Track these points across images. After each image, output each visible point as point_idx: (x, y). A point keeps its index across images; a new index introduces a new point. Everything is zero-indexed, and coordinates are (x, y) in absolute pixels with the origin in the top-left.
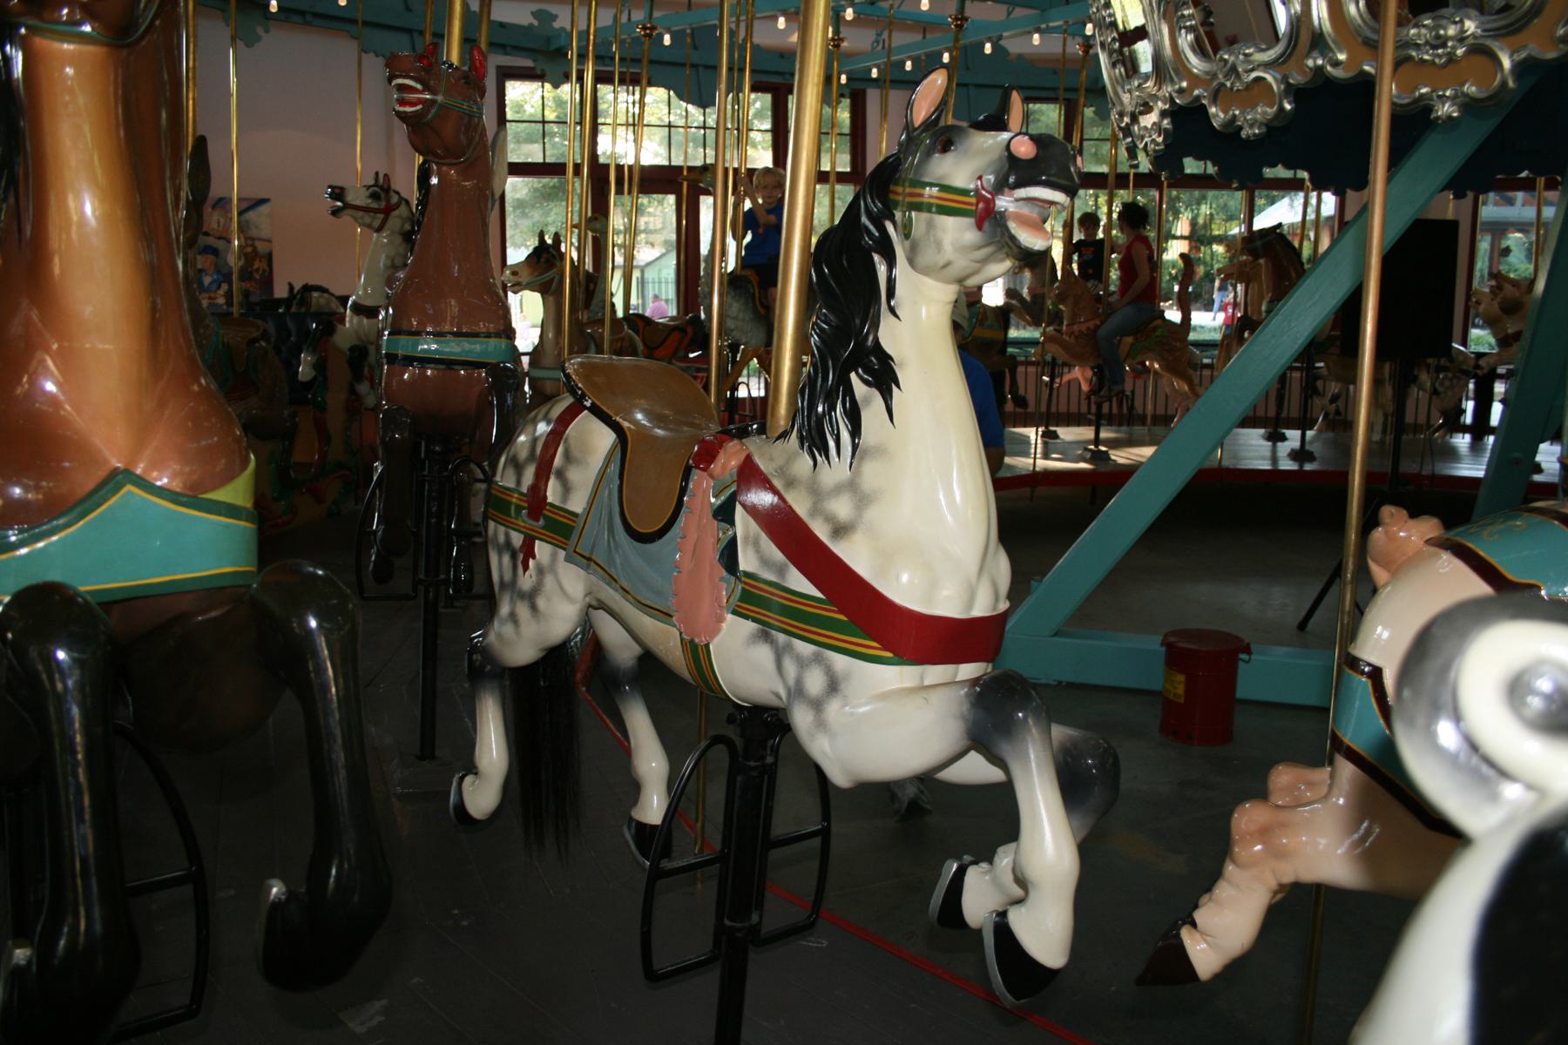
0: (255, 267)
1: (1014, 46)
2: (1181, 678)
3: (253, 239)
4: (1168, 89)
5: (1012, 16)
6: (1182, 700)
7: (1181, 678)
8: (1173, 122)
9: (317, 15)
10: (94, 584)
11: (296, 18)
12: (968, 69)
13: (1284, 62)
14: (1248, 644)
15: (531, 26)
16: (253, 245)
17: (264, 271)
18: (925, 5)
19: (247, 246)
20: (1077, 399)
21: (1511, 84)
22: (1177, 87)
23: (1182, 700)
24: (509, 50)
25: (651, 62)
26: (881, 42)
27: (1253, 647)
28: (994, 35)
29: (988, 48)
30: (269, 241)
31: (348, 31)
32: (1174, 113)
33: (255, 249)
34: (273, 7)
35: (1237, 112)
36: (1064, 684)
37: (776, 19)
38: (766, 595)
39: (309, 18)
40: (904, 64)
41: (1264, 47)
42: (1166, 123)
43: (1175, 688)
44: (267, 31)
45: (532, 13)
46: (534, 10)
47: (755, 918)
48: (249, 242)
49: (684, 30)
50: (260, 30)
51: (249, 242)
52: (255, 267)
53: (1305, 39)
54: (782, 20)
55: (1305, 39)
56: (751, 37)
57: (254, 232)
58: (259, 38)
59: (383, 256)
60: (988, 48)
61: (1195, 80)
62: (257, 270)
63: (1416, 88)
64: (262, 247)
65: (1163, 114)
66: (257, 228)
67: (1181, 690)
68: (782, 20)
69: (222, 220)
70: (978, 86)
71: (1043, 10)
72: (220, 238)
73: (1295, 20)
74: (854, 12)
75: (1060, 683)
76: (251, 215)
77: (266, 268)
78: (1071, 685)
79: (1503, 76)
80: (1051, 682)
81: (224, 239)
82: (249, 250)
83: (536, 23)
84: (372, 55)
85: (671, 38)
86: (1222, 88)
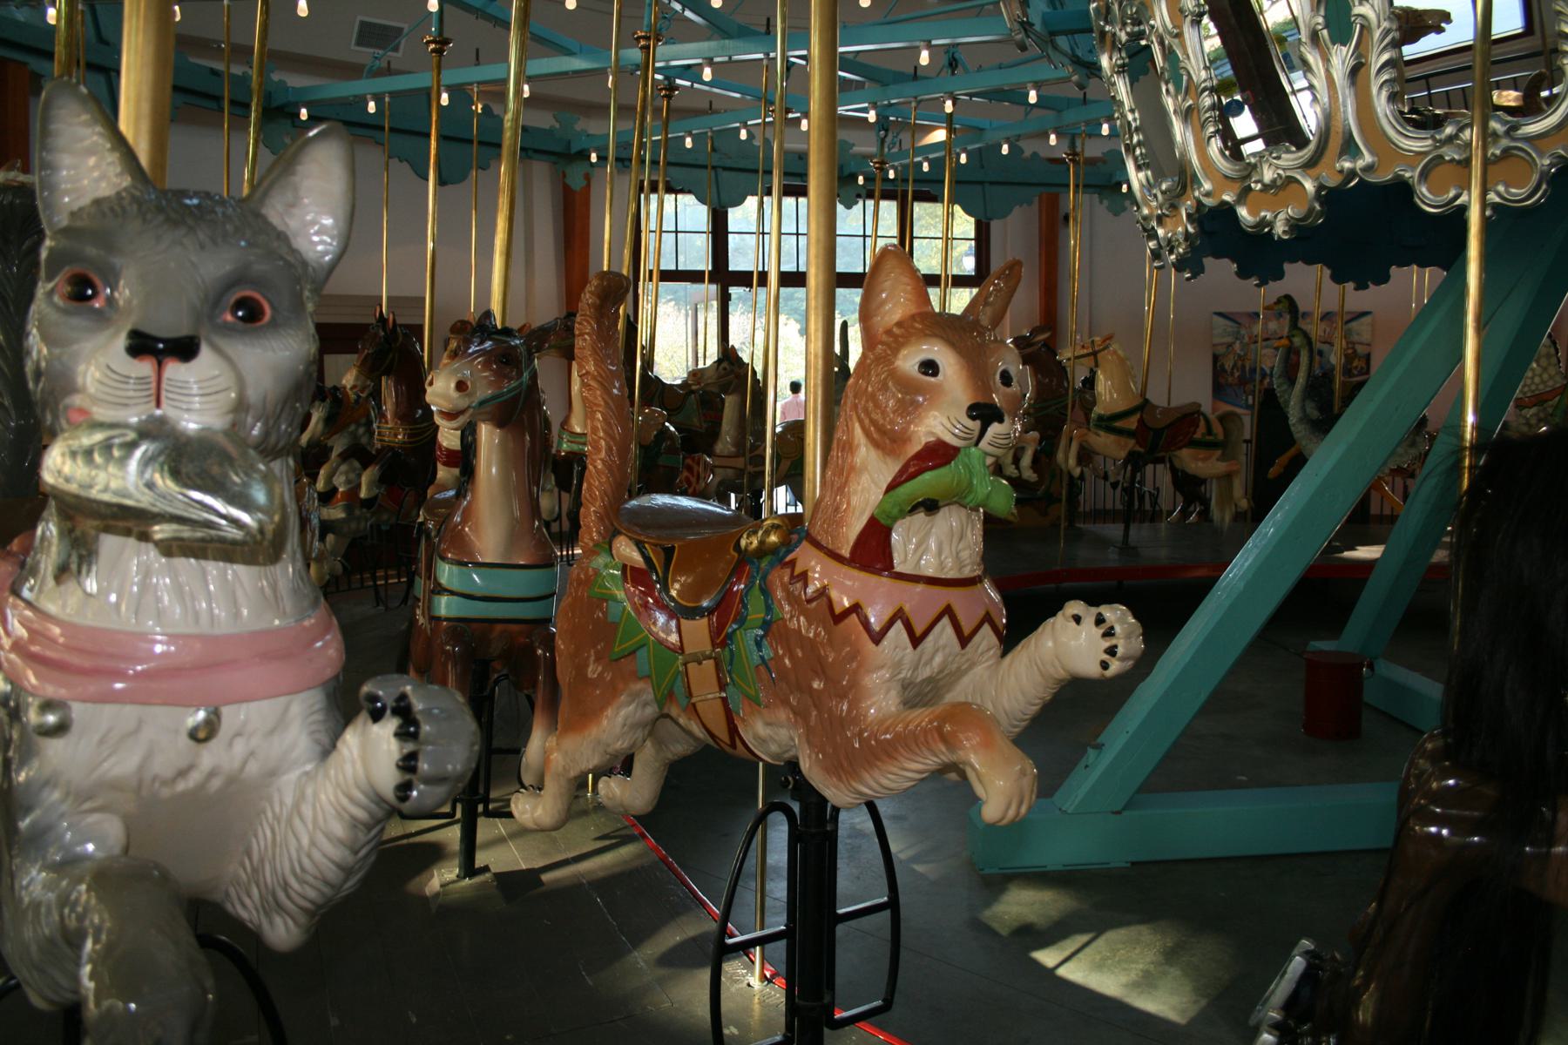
0: (1354, 364)
1: (1028, 148)
3: (1354, 343)
5: (1028, 117)
16: (1353, 348)
17: (1362, 368)
19: (1348, 348)
25: (705, 167)
26: (898, 144)
29: (1005, 149)
30: (1369, 345)
33: (1355, 351)
38: (388, 846)
40: (683, 139)
48: (1350, 346)
49: (706, 133)
51: (1350, 346)
52: (1354, 364)
53: (1335, 143)
54: (1053, 137)
55: (1335, 143)
57: (1355, 338)
60: (1005, 149)
62: (1356, 367)
64: (1360, 349)
66: (1358, 334)
68: (1053, 137)
69: (1328, 330)
70: (992, 183)
71: (1059, 111)
72: (1324, 343)
76: (1354, 324)
77: (1364, 365)
81: (1329, 343)
82: (1350, 351)
84: (396, 160)
85: (693, 141)
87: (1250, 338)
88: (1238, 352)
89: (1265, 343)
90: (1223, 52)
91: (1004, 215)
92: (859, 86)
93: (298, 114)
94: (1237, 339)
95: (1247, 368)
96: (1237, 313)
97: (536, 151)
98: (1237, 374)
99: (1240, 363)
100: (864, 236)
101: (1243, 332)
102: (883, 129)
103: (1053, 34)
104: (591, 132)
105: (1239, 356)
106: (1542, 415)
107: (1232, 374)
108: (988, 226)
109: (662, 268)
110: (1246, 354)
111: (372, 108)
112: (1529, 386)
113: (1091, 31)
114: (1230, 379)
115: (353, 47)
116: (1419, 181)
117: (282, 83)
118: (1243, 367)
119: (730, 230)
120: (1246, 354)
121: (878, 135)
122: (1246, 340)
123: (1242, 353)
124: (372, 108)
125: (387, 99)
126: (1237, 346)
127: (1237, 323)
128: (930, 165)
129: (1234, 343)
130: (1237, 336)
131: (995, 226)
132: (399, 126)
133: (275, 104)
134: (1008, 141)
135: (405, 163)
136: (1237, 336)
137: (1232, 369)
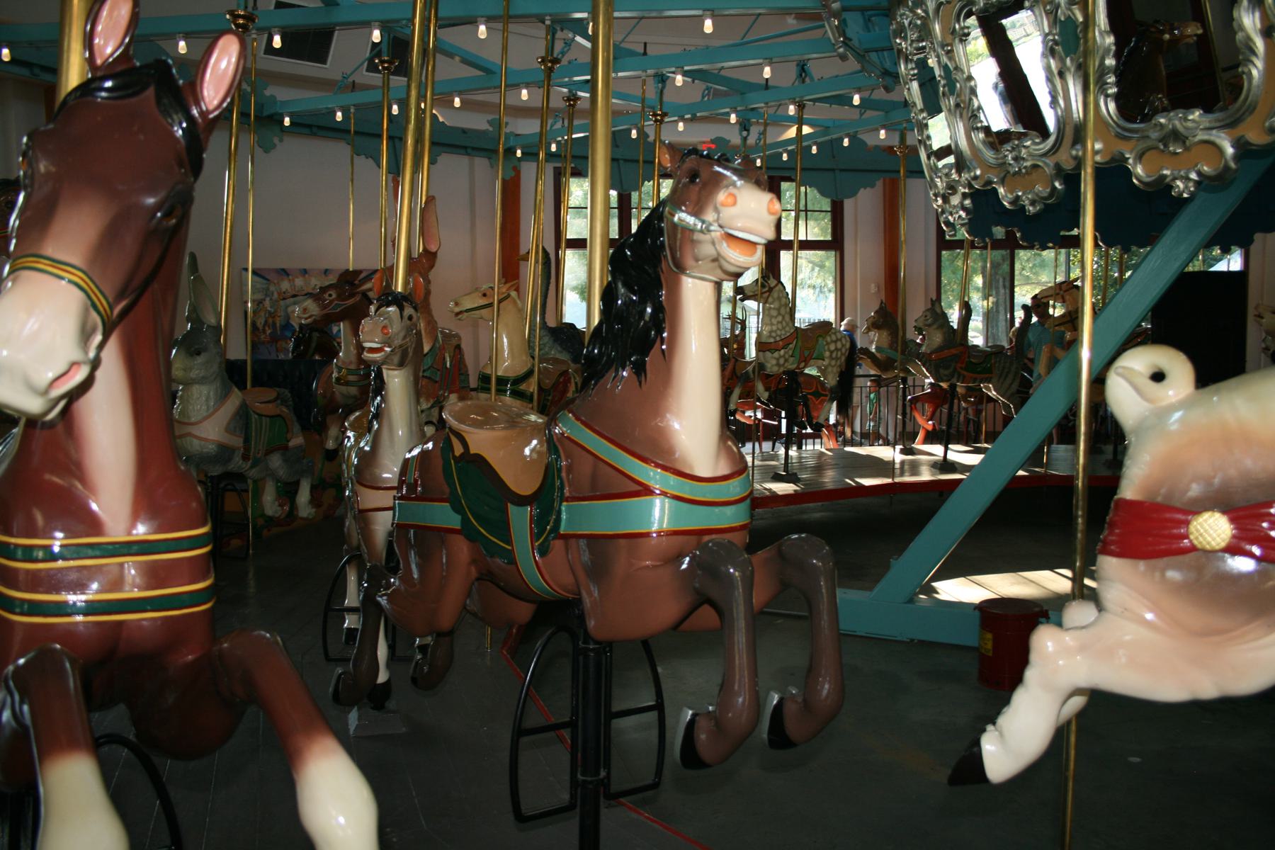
2: (989, 636)
4: (965, 176)
5: (864, 117)
6: (990, 654)
7: (989, 636)
8: (973, 202)
9: (320, 127)
10: (527, 533)
11: (307, 131)
12: (834, 157)
13: (1054, 153)
14: (1047, 611)
15: (485, 132)
18: (395, 111)
20: (992, 412)
21: (1233, 165)
22: (972, 174)
23: (990, 654)
24: (469, 151)
27: (1050, 613)
28: (851, 131)
29: (846, 142)
31: (345, 139)
32: (974, 195)
34: (339, 118)
35: (1020, 194)
36: (916, 641)
37: (878, 130)
39: (315, 130)
40: (629, 131)
41: (1037, 141)
42: (967, 202)
43: (986, 644)
44: (281, 141)
45: (488, 122)
46: (490, 119)
47: (603, 774)
50: (276, 140)
54: (883, 132)
56: (660, 136)
58: (274, 146)
59: (873, 285)
60: (846, 142)
61: (986, 166)
63: (1162, 169)
65: (965, 196)
67: (989, 645)
68: (883, 132)
70: (626, 160)
71: (887, 112)
73: (1061, 120)
74: (737, 116)
75: (912, 640)
78: (922, 642)
79: (1226, 159)
80: (905, 640)
83: (491, 129)
86: (1008, 175)
87: (279, 294)
88: (269, 309)
89: (756, 293)
90: (1113, 68)
91: (853, 194)
92: (725, 94)
93: (283, 121)
94: (266, 295)
95: (278, 325)
96: (265, 269)
97: (474, 149)
98: (269, 332)
99: (270, 320)
100: (806, 211)
101: (272, 288)
102: (745, 130)
103: (868, 51)
104: (519, 132)
105: (270, 312)
106: (787, 356)
107: (264, 332)
108: (842, 203)
109: (567, 238)
110: (276, 311)
111: (339, 116)
112: (841, 350)
113: (893, 49)
114: (262, 337)
115: (365, 73)
116: (1135, 164)
117: (273, 97)
118: (274, 324)
119: (829, 214)
120: (276, 311)
121: (741, 135)
122: (276, 296)
123: (272, 310)
124: (339, 116)
125: (352, 110)
126: (267, 303)
127: (268, 280)
128: (788, 155)
129: (265, 300)
130: (267, 293)
131: (848, 204)
132: (361, 130)
133: (266, 113)
134: (848, 135)
135: (370, 159)
136: (267, 293)
137: (264, 326)
